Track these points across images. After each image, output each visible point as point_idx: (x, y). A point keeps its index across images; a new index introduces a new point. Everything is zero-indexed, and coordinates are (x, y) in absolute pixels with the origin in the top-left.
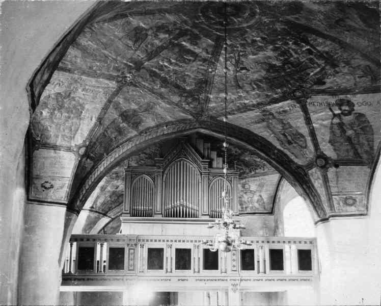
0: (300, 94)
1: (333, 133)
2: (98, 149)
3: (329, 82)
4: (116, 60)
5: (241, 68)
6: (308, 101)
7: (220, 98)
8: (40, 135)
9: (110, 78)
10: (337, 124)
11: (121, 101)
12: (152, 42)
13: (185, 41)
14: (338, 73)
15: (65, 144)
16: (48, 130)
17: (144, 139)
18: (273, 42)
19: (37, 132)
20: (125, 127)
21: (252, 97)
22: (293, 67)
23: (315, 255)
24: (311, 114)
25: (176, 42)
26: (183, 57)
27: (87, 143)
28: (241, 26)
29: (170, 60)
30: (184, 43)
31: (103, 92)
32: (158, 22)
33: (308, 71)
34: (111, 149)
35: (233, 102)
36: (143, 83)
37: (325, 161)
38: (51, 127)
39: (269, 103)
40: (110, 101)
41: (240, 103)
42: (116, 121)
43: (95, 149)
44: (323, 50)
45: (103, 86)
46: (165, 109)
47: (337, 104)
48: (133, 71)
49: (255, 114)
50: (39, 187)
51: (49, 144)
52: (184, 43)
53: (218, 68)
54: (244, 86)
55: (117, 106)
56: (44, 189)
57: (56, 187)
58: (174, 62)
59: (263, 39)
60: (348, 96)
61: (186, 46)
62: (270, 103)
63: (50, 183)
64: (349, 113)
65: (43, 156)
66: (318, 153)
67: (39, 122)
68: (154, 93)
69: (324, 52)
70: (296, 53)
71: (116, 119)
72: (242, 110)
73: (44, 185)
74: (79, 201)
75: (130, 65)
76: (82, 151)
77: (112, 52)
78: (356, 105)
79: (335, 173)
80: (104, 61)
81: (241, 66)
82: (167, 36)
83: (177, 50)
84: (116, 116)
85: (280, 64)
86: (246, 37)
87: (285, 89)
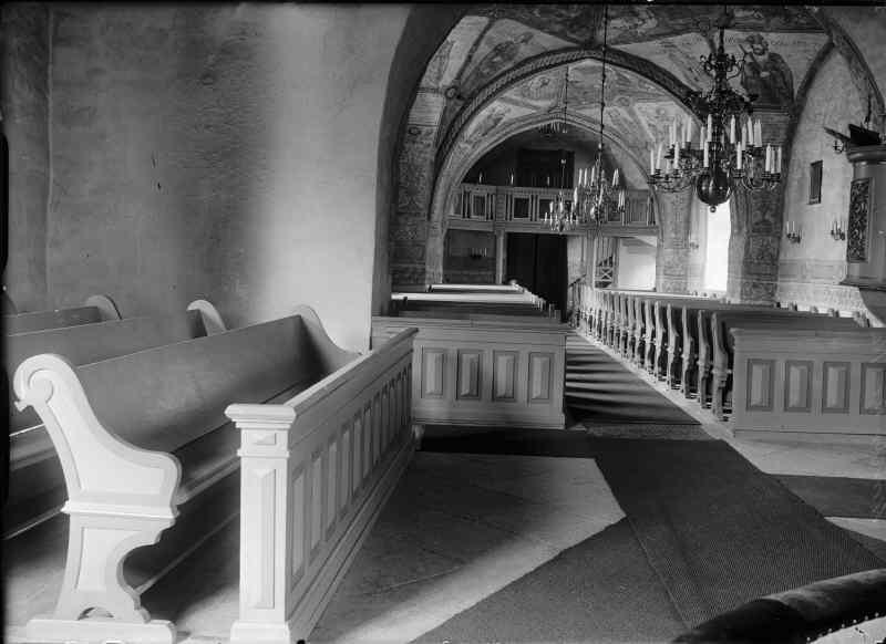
2: (468, 88)
23: (548, 325)
40: (481, 37)
64: (763, 53)
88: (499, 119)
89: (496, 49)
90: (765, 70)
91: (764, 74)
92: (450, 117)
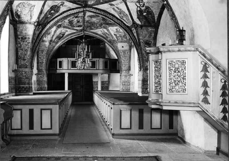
27: (38, 21)
64: (143, 6)
76: (36, 24)
88: (64, 34)
89: (51, 8)
90: (145, 12)
91: (145, 14)
92: (37, 32)
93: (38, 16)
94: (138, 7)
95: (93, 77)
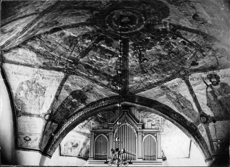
0: (183, 73)
1: (208, 97)
3: (201, 63)
4: (60, 58)
5: (143, 59)
6: (190, 77)
7: (134, 80)
8: (21, 108)
9: (59, 70)
10: (210, 92)
11: (70, 85)
12: (82, 45)
13: (103, 44)
14: (204, 56)
15: (37, 113)
16: (25, 105)
17: (90, 109)
18: (159, 40)
19: (19, 106)
20: (76, 102)
21: (154, 78)
22: (175, 55)
24: (193, 86)
25: (97, 45)
26: (104, 55)
27: (50, 112)
28: (136, 30)
29: (96, 57)
30: (102, 45)
31: (56, 79)
32: (82, 32)
33: (186, 56)
34: (70, 116)
35: (142, 82)
36: (82, 73)
37: (206, 118)
38: (26, 102)
39: (164, 81)
40: (62, 85)
41: (147, 82)
42: (69, 98)
43: (57, 116)
44: (192, 40)
45: (55, 75)
46: (100, 90)
47: (208, 78)
48: (73, 65)
49: (157, 90)
50: (23, 139)
51: (26, 113)
52: (102, 45)
53: (129, 61)
54: (147, 71)
55: (67, 88)
56: (25, 141)
57: (32, 139)
58: (99, 58)
59: (152, 38)
60: (215, 71)
61: (104, 47)
62: (165, 81)
63: (29, 137)
64: (217, 84)
65: (23, 120)
66: (201, 113)
67: (19, 99)
68: (90, 79)
69: (193, 42)
70: (175, 44)
71: (68, 96)
72: (149, 87)
73: (25, 138)
74: (50, 149)
75: (70, 62)
76: (47, 117)
77: (57, 53)
78: (221, 78)
79: (214, 127)
80: (52, 59)
81: (143, 58)
82: (90, 41)
83: (99, 50)
84: (68, 95)
85: (167, 54)
86: (141, 38)
87: (173, 71)
93: (9, 64)
94: (208, 86)
95: (26, 165)
